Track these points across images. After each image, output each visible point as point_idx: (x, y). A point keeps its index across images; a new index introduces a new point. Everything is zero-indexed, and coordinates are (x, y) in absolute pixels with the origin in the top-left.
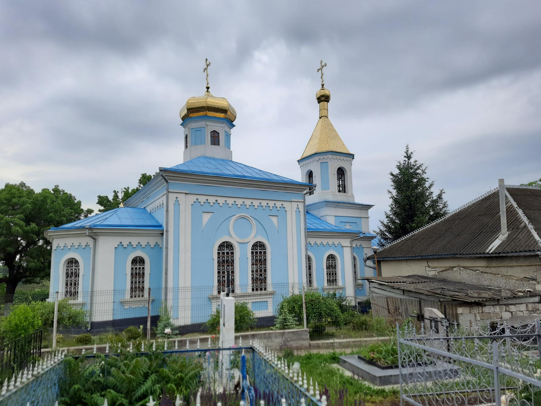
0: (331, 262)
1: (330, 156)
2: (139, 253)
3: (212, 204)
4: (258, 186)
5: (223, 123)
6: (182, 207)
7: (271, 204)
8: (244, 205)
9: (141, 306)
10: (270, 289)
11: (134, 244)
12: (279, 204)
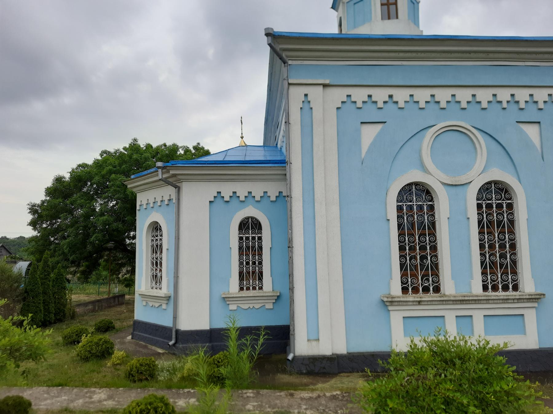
2: (250, 211)
3: (380, 104)
4: (487, 56)
6: (317, 114)
7: (522, 95)
8: (454, 101)
9: (257, 306)
10: (528, 286)
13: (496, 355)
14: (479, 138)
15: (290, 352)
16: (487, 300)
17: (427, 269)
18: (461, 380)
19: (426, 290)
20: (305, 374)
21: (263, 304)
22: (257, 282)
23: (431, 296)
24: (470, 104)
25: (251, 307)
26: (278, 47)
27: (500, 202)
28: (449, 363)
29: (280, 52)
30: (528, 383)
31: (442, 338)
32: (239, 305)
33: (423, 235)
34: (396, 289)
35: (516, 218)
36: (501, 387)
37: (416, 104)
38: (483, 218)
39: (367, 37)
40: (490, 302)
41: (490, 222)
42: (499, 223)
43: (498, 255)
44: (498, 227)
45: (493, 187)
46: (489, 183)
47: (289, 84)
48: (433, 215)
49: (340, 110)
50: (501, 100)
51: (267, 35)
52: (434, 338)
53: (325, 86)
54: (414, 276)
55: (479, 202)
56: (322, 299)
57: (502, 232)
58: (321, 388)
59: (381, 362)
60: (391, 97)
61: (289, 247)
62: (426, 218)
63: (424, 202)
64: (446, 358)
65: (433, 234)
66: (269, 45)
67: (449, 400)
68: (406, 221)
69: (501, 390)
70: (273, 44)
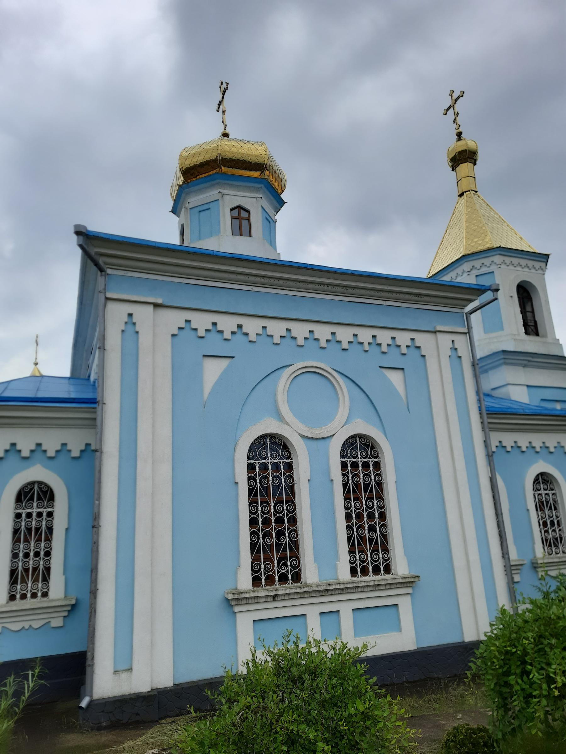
0: (543, 492)
1: (498, 259)
2: (37, 473)
3: (227, 335)
4: (346, 291)
5: (257, 190)
6: (145, 340)
7: (384, 337)
8: (311, 338)
9: (36, 625)
10: (401, 568)
11: (25, 447)
12: (403, 339)
13: (354, 663)
14: (341, 383)
15: (85, 696)
16: (356, 587)
17: (285, 550)
18: (309, 705)
19: (283, 579)
20: (106, 728)
21: (47, 621)
22: (40, 585)
23: (290, 587)
24: (330, 343)
25: (27, 627)
26: (93, 251)
27: (366, 460)
28: (297, 681)
29: (96, 257)
30: (389, 698)
31: (291, 646)
32: (7, 625)
33: (279, 502)
34: (245, 581)
35: (384, 481)
36: (356, 709)
37: (269, 339)
38: (348, 480)
39: (211, 253)
40: (360, 590)
41: (357, 485)
42: (367, 486)
43: (366, 528)
44: (365, 492)
45: (358, 442)
46: (353, 437)
47: (107, 299)
48: (291, 477)
49: (176, 338)
50: (362, 341)
51: (78, 233)
52: (282, 647)
53: (156, 306)
54: (268, 560)
55: (344, 460)
56: (141, 603)
57: (370, 498)
58: (129, 747)
59: (209, 693)
60: (240, 327)
61: (93, 527)
62: (283, 480)
63: (281, 459)
64: (293, 673)
65: (291, 501)
66: (81, 246)
67: (293, 737)
68: (258, 484)
69: (357, 712)
70: (85, 247)
